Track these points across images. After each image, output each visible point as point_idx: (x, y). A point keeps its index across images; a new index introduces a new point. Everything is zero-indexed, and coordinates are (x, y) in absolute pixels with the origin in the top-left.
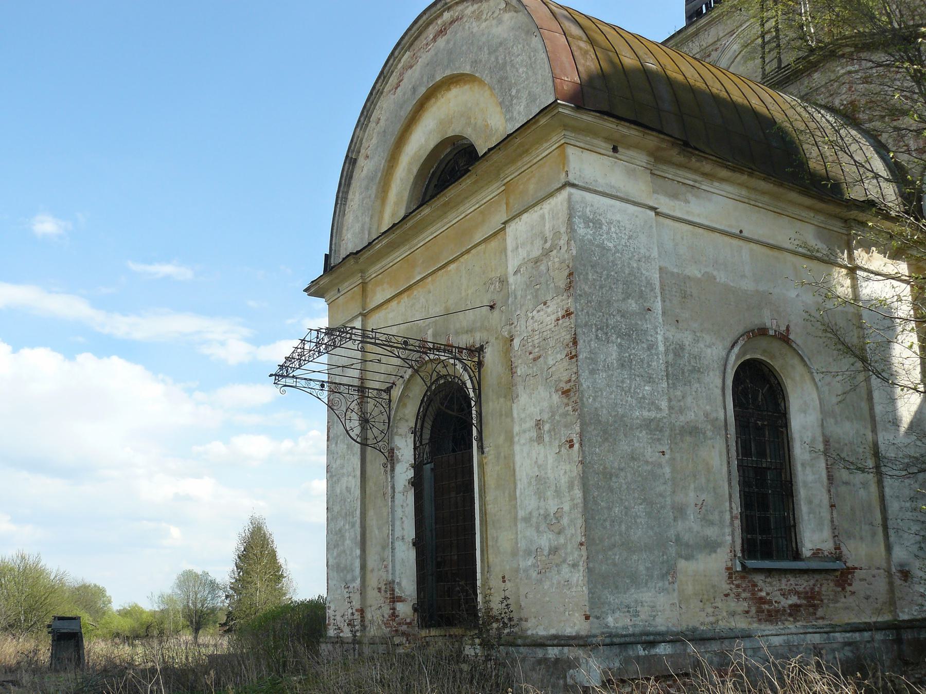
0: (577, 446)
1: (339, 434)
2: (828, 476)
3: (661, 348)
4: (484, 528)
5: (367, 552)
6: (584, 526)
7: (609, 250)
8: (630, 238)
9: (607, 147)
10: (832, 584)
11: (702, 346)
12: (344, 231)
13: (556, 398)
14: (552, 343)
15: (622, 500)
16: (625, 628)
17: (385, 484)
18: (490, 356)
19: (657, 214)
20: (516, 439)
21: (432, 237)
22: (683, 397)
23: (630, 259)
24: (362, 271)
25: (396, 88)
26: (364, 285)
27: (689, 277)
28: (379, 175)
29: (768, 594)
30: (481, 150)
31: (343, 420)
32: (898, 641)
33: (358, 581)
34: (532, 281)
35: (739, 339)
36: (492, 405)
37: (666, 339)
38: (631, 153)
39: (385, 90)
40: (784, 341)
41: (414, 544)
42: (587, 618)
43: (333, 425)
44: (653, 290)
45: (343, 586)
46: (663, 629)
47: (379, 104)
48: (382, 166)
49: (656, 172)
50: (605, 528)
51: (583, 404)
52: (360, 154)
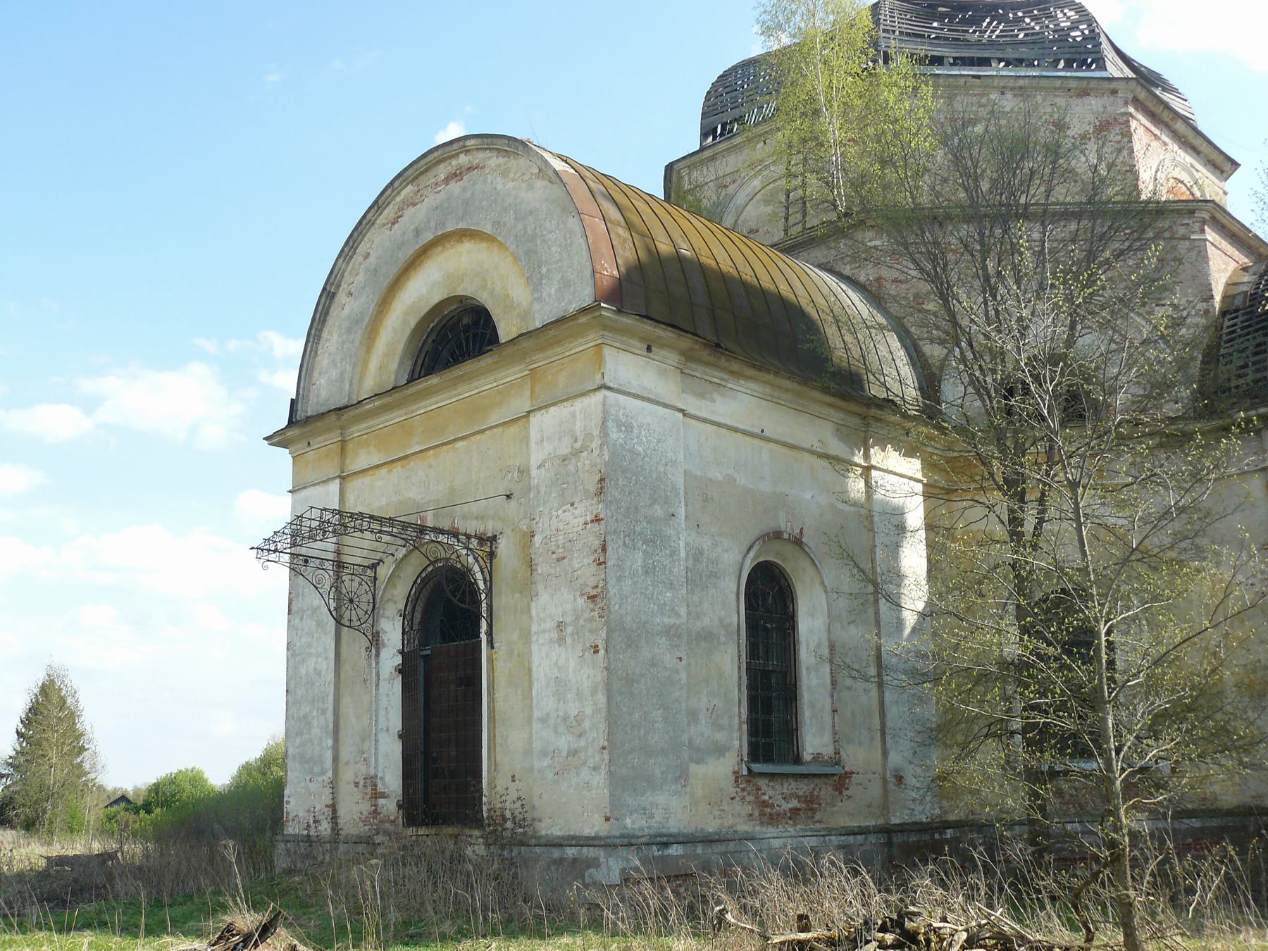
0: (602, 652)
1: (305, 608)
2: (832, 681)
3: (683, 554)
4: (492, 725)
5: (341, 742)
6: (606, 732)
7: (639, 454)
8: (659, 441)
9: (640, 347)
10: (830, 789)
11: (720, 551)
12: (316, 374)
13: (581, 602)
14: (578, 546)
15: (641, 705)
16: (642, 829)
17: (367, 670)
18: (504, 548)
19: (684, 415)
20: (534, 638)
21: (436, 406)
22: (700, 603)
23: (657, 463)
24: (342, 428)
25: (393, 224)
26: (343, 444)
27: (711, 480)
28: (367, 319)
29: (770, 798)
30: (506, 331)
31: (327, 600)
32: (889, 844)
33: (330, 774)
34: (558, 479)
35: (754, 543)
36: (505, 600)
37: (687, 544)
38: (664, 352)
39: (377, 221)
40: (797, 544)
41: (400, 736)
42: (607, 819)
43: (297, 596)
44: (677, 495)
45: (308, 779)
46: (676, 831)
47: (368, 235)
48: (371, 310)
49: (687, 371)
50: (626, 733)
51: (610, 611)
52: (341, 289)
